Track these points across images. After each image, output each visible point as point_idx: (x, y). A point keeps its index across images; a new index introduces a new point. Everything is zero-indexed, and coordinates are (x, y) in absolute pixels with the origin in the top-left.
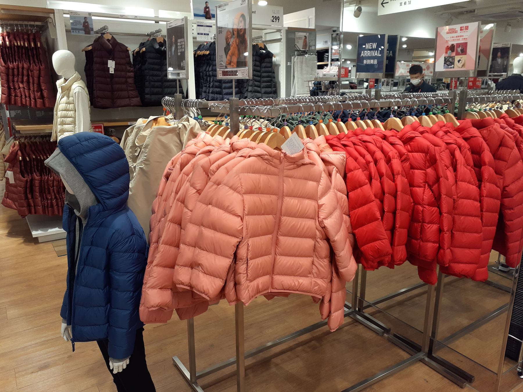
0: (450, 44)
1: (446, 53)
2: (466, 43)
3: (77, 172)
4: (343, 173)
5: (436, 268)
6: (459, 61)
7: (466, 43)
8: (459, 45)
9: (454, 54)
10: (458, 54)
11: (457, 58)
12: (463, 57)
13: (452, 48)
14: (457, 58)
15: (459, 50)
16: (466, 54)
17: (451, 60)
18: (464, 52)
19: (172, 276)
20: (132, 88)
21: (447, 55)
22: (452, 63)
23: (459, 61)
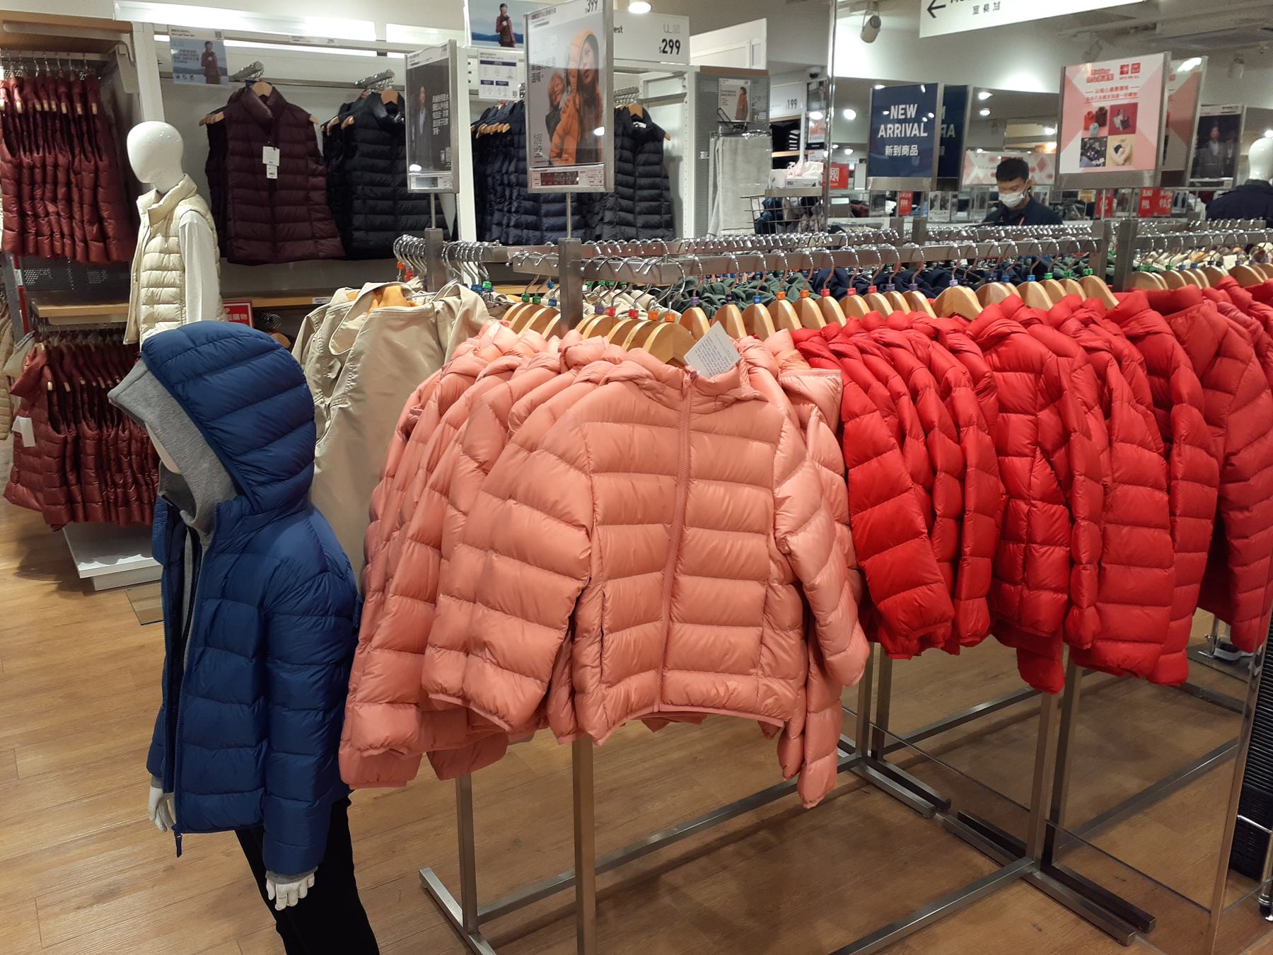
0: (1095, 107)
1: (1086, 128)
2: (1135, 105)
3: (187, 420)
4: (834, 422)
5: (1061, 654)
6: (1117, 149)
7: (1135, 105)
8: (1116, 110)
9: (1104, 132)
10: (1114, 131)
11: (1113, 141)
12: (1128, 140)
13: (1100, 117)
14: (1113, 141)
15: (1118, 121)
16: (1133, 132)
17: (1097, 145)
18: (1129, 126)
19: (418, 672)
20: (320, 215)
21: (1088, 135)
22: (1101, 154)
23: (1117, 149)
